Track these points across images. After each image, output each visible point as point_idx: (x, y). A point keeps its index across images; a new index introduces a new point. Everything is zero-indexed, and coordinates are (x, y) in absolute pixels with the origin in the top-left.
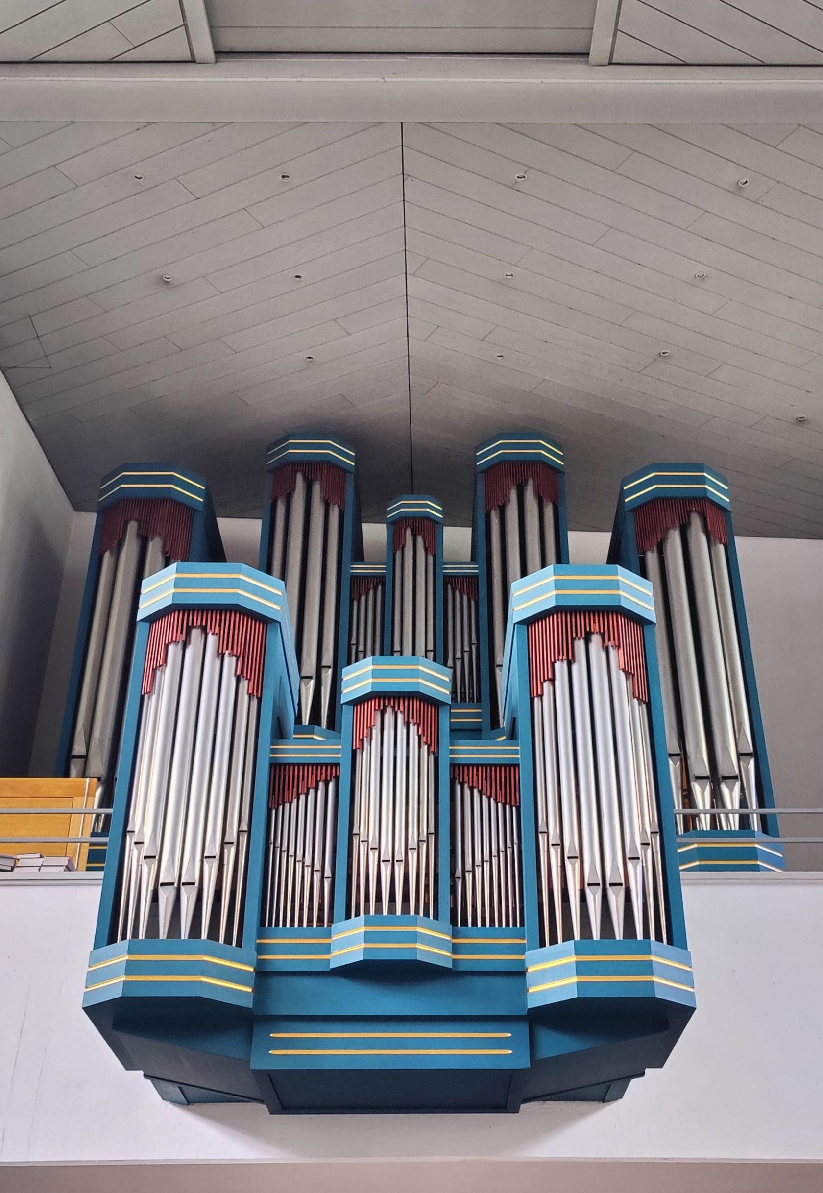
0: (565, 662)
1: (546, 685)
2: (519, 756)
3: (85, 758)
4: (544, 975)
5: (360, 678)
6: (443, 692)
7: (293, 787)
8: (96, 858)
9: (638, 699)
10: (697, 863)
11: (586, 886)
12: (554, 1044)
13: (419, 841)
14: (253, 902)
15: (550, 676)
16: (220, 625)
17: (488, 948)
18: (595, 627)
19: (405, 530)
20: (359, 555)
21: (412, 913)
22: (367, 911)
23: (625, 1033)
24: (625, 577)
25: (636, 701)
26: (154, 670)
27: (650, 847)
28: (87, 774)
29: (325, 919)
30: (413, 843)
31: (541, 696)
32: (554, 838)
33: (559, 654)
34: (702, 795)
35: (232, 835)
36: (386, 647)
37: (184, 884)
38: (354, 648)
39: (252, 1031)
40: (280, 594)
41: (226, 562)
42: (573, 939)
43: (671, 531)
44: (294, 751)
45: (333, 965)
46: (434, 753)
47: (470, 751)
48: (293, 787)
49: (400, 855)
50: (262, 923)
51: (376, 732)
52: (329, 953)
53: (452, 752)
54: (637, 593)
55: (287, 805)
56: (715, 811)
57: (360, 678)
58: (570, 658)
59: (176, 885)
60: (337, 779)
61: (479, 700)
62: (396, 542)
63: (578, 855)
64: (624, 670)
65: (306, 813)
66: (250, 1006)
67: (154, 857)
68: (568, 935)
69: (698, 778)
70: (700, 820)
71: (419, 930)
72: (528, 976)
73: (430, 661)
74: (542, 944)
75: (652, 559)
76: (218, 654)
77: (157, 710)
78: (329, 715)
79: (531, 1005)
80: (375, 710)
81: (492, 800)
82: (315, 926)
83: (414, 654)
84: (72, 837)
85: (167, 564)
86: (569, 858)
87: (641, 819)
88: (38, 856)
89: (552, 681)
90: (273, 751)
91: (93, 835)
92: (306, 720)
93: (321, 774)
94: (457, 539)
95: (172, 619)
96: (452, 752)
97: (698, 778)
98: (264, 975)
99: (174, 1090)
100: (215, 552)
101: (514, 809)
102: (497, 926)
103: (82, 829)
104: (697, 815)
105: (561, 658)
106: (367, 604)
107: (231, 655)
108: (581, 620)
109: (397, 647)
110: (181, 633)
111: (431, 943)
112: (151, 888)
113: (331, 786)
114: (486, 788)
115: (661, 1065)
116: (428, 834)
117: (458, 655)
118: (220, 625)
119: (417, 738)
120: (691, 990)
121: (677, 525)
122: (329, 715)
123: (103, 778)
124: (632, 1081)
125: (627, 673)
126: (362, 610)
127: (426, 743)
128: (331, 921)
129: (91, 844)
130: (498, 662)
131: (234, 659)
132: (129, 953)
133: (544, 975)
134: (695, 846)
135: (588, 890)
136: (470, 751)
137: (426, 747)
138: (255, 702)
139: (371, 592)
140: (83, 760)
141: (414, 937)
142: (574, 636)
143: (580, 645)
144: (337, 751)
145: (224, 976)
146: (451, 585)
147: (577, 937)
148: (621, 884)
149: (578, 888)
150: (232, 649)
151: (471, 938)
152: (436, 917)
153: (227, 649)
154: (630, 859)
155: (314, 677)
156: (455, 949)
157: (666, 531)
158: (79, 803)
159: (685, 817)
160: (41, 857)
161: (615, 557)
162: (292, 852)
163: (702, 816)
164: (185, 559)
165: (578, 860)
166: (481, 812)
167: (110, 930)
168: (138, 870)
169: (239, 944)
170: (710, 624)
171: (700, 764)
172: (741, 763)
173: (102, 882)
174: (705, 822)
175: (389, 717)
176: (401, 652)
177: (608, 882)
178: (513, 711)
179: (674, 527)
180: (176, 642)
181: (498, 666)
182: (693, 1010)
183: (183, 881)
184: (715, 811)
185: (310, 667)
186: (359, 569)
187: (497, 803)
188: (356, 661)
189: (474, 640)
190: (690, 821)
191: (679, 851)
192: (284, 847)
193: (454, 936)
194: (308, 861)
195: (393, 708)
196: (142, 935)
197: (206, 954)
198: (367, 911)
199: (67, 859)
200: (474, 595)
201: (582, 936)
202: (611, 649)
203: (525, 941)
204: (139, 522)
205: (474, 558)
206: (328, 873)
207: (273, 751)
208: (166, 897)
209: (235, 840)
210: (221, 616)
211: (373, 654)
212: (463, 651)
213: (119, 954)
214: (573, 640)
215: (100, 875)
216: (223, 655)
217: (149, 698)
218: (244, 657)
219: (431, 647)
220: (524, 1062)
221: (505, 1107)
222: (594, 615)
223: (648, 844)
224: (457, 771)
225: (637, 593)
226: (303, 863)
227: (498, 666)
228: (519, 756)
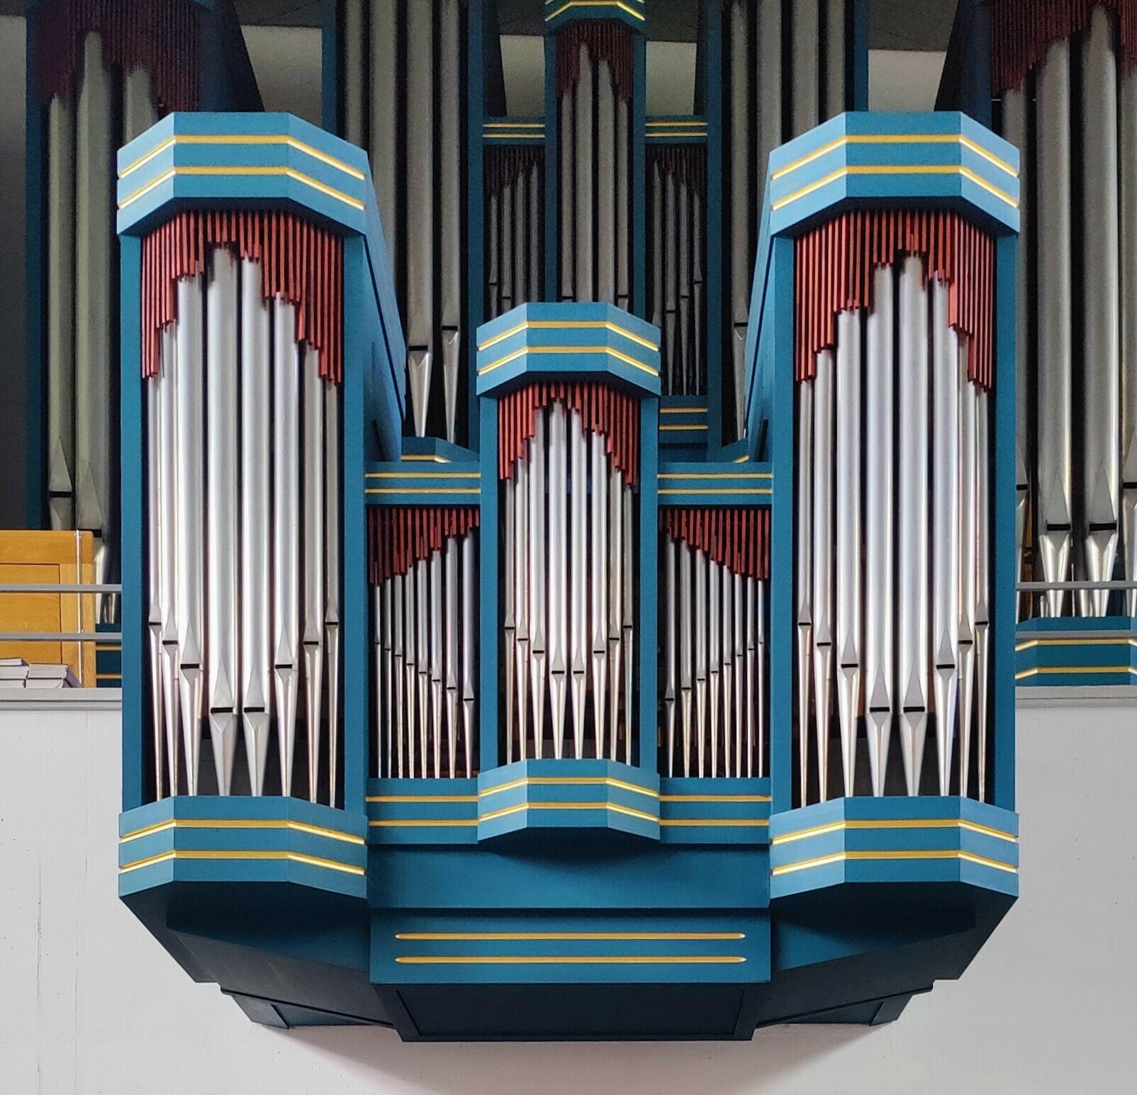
0: (857, 312)
1: (821, 357)
2: (771, 491)
3: (72, 495)
4: (796, 852)
5: (507, 346)
6: (646, 372)
7: (406, 547)
8: (108, 665)
9: (976, 382)
10: (1035, 671)
11: (868, 711)
12: (806, 949)
13: (609, 639)
14: (356, 738)
15: (829, 341)
16: (262, 242)
17: (715, 810)
18: (912, 242)
19: (579, 49)
20: (497, 106)
21: (599, 755)
22: (531, 753)
23: (910, 931)
24: (972, 137)
25: (971, 387)
26: (158, 331)
27: (972, 647)
28: (78, 524)
29: (468, 766)
30: (599, 642)
31: (812, 379)
32: (821, 633)
33: (847, 297)
34: (1054, 556)
35: (315, 629)
36: (549, 288)
37: (248, 710)
38: (494, 290)
39: (369, 936)
40: (362, 177)
41: (262, 109)
42: (843, 794)
43: (1054, 48)
44: (409, 482)
45: (481, 836)
46: (632, 487)
47: (693, 483)
48: (406, 547)
49: (579, 662)
50: (372, 772)
51: (536, 448)
52: (475, 817)
53: (662, 484)
54: (987, 169)
55: (399, 579)
56: (1072, 585)
57: (507, 346)
58: (866, 304)
59: (235, 711)
60: (476, 532)
61: (704, 391)
62: (561, 74)
63: (858, 661)
64: (956, 327)
65: (430, 591)
66: (363, 894)
67: (197, 666)
68: (836, 789)
69: (1052, 528)
70: (1046, 599)
71: (610, 782)
72: (773, 852)
73: (622, 311)
74: (796, 804)
75: (1014, 104)
76: (264, 299)
77: (171, 406)
78: (460, 418)
79: (774, 895)
80: (534, 408)
81: (725, 568)
82: (452, 776)
83: (596, 298)
84: (67, 630)
85: (161, 115)
86: (844, 666)
87: (962, 600)
88: (19, 662)
89: (833, 349)
90: (371, 483)
91: (99, 628)
92: (421, 430)
93: (450, 524)
94: (670, 65)
95: (176, 230)
96: (662, 484)
97: (1052, 528)
98: (381, 851)
99: (266, 1008)
100: (242, 93)
101: (760, 583)
102: (728, 776)
103: (81, 616)
104: (1044, 593)
105: (850, 304)
106: (516, 199)
107: (286, 300)
108: (888, 228)
109: (567, 290)
110: (197, 258)
111: (628, 802)
112: (198, 716)
113: (467, 544)
114: (717, 550)
115: (956, 975)
116: (623, 627)
117: (671, 305)
118: (262, 242)
119: (604, 459)
120: (1014, 871)
121: (1066, 29)
122: (460, 418)
123: (105, 531)
124: (914, 997)
125: (961, 332)
126: (505, 223)
127: (619, 468)
128: (476, 768)
129: (99, 643)
130: (738, 316)
131: (292, 308)
132: (177, 817)
133: (796, 852)
134: (1036, 643)
135: (870, 719)
136: (693, 483)
137: (619, 475)
138: (333, 393)
139: (520, 180)
140: (68, 500)
141: (603, 793)
142: (875, 260)
143: (884, 277)
144: (473, 483)
145: (319, 851)
146: (659, 164)
147: (849, 792)
148: (922, 709)
149: (855, 714)
150: (287, 289)
151: (688, 794)
152: (636, 762)
153: (278, 289)
154: (939, 667)
155: (430, 348)
156: (665, 811)
157: (1047, 43)
158: (70, 575)
159: (1024, 595)
160: (24, 664)
161: (952, 96)
162: (410, 659)
163: (1051, 593)
164: (194, 104)
165: (858, 670)
166: (709, 588)
167: (144, 782)
168: (175, 690)
169: (340, 804)
170: (1103, 240)
171: (1058, 505)
172: (1124, 501)
173: (120, 705)
174: (1054, 605)
175: (557, 420)
176: (574, 298)
177: (902, 705)
178: (764, 408)
179: (1059, 37)
180: (190, 276)
181: (737, 325)
182: (1015, 898)
183: (245, 705)
184: (1072, 585)
185: (422, 328)
186: (500, 131)
187: (732, 574)
188: (500, 313)
189: (697, 275)
190: (1032, 601)
191: (1017, 649)
192: (399, 650)
193: (663, 791)
194: (436, 673)
195: (564, 402)
196: (192, 789)
197: (291, 819)
198: (531, 753)
199: (64, 667)
200: (700, 180)
201: (857, 791)
202: (937, 284)
203: (770, 799)
204: (104, 36)
205: (700, 108)
206: (468, 692)
207: (371, 483)
208: (221, 730)
209: (320, 638)
210: (261, 222)
211: (527, 299)
212: (678, 296)
213: (161, 820)
214: (873, 267)
215: (116, 693)
216: (272, 300)
217: (156, 384)
218: (308, 305)
219: (624, 289)
220: (762, 974)
221: (733, 1033)
222: (912, 218)
223: (970, 642)
224: (669, 520)
225: (987, 169)
226: (430, 676)
227: (737, 325)
228: (771, 491)
